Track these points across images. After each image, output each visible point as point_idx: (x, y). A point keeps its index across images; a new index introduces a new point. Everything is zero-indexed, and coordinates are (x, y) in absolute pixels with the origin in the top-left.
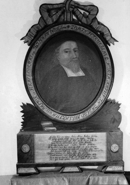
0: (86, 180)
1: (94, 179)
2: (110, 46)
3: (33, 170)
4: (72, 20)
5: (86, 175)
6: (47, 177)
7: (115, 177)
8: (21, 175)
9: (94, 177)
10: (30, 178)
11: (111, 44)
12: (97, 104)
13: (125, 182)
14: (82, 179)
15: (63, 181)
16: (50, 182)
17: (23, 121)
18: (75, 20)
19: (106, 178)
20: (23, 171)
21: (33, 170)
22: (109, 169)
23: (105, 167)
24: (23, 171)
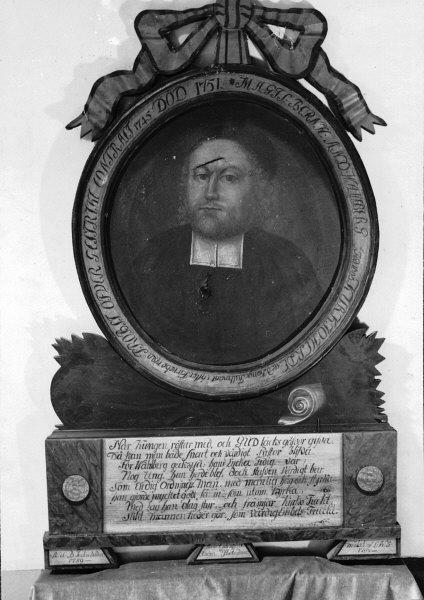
0: (284, 588)
1: (313, 582)
2: (359, 139)
3: (94, 557)
4: (245, 62)
5: (285, 571)
6: (155, 576)
7: (382, 577)
8: (57, 571)
9: (312, 576)
10: (99, 579)
11: (364, 133)
12: (323, 335)
13: (414, 591)
14: (269, 582)
15: (206, 591)
16: (166, 593)
17: (382, 406)
18: (257, 60)
19: (350, 580)
20: (65, 557)
21: (94, 557)
22: (348, 550)
23: (338, 542)
24: (65, 557)
